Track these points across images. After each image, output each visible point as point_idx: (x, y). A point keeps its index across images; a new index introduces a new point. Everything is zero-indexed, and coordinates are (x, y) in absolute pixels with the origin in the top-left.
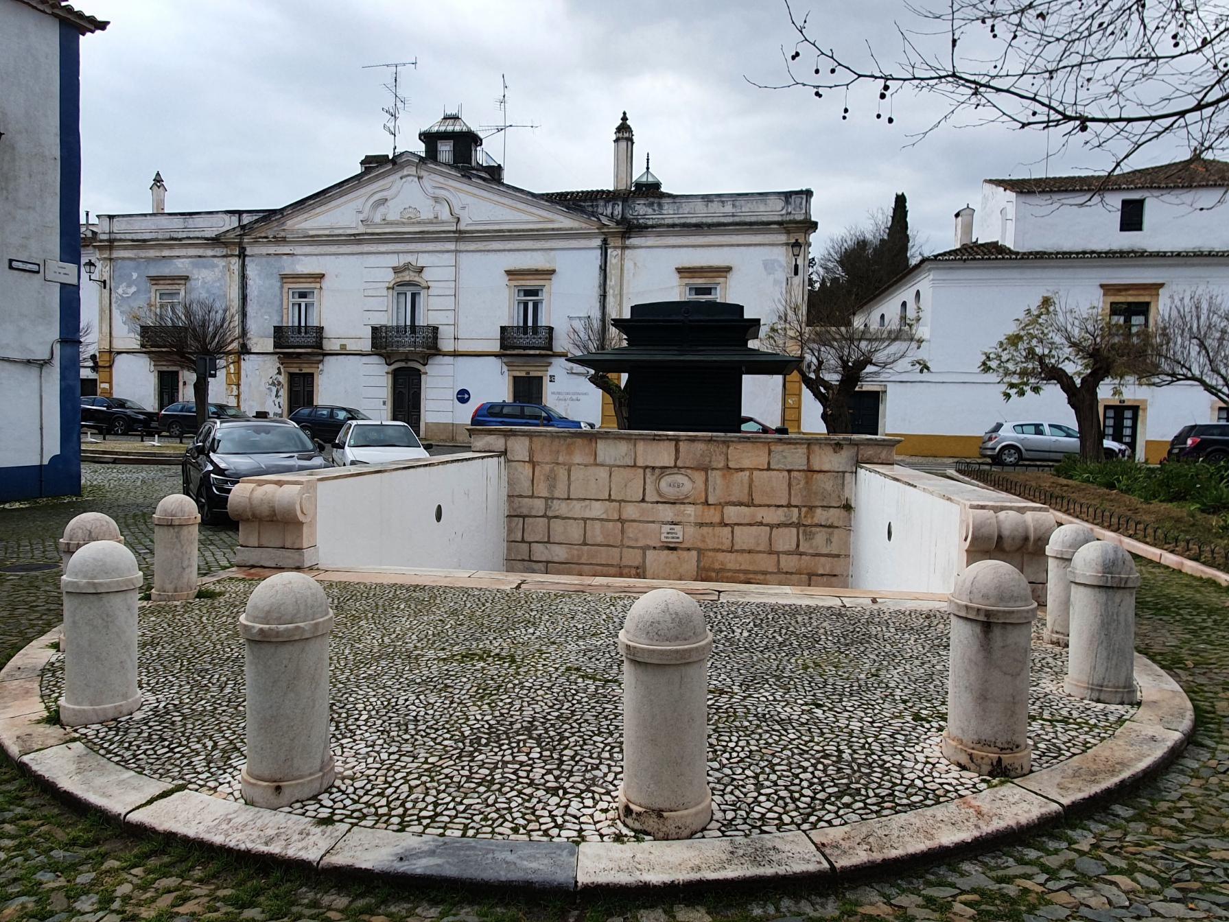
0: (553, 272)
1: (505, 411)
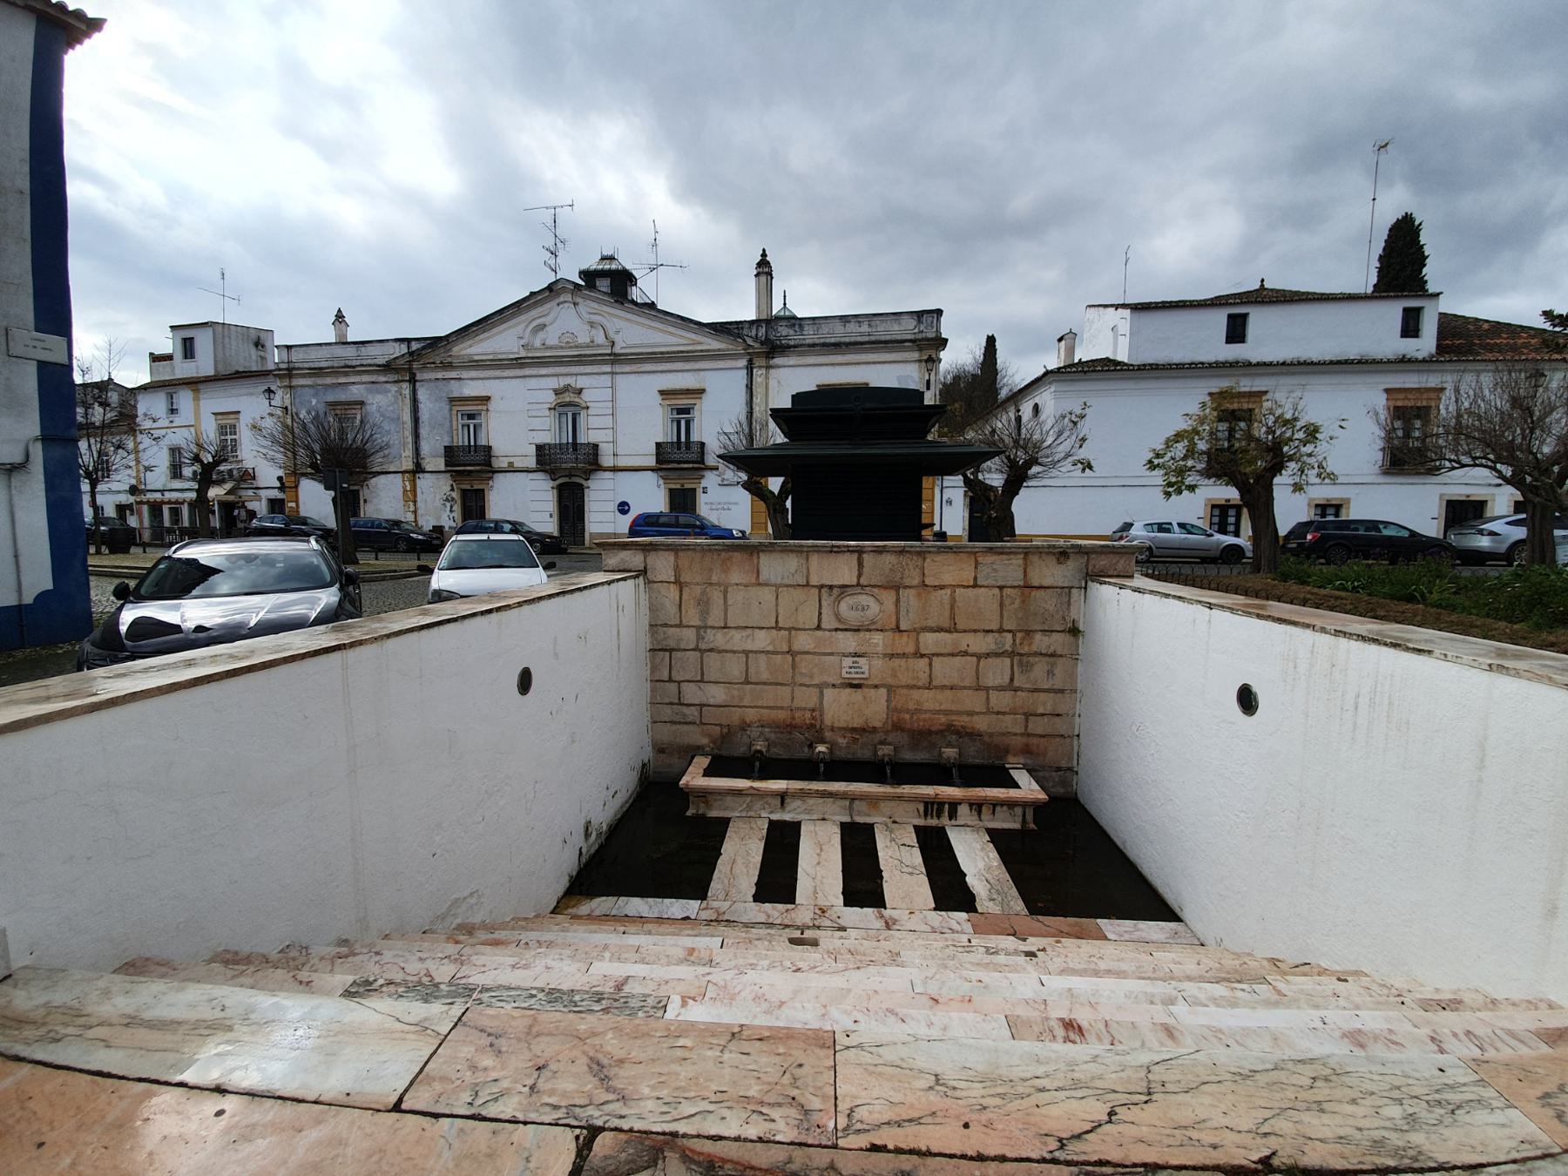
0: (703, 391)
1: (662, 520)
